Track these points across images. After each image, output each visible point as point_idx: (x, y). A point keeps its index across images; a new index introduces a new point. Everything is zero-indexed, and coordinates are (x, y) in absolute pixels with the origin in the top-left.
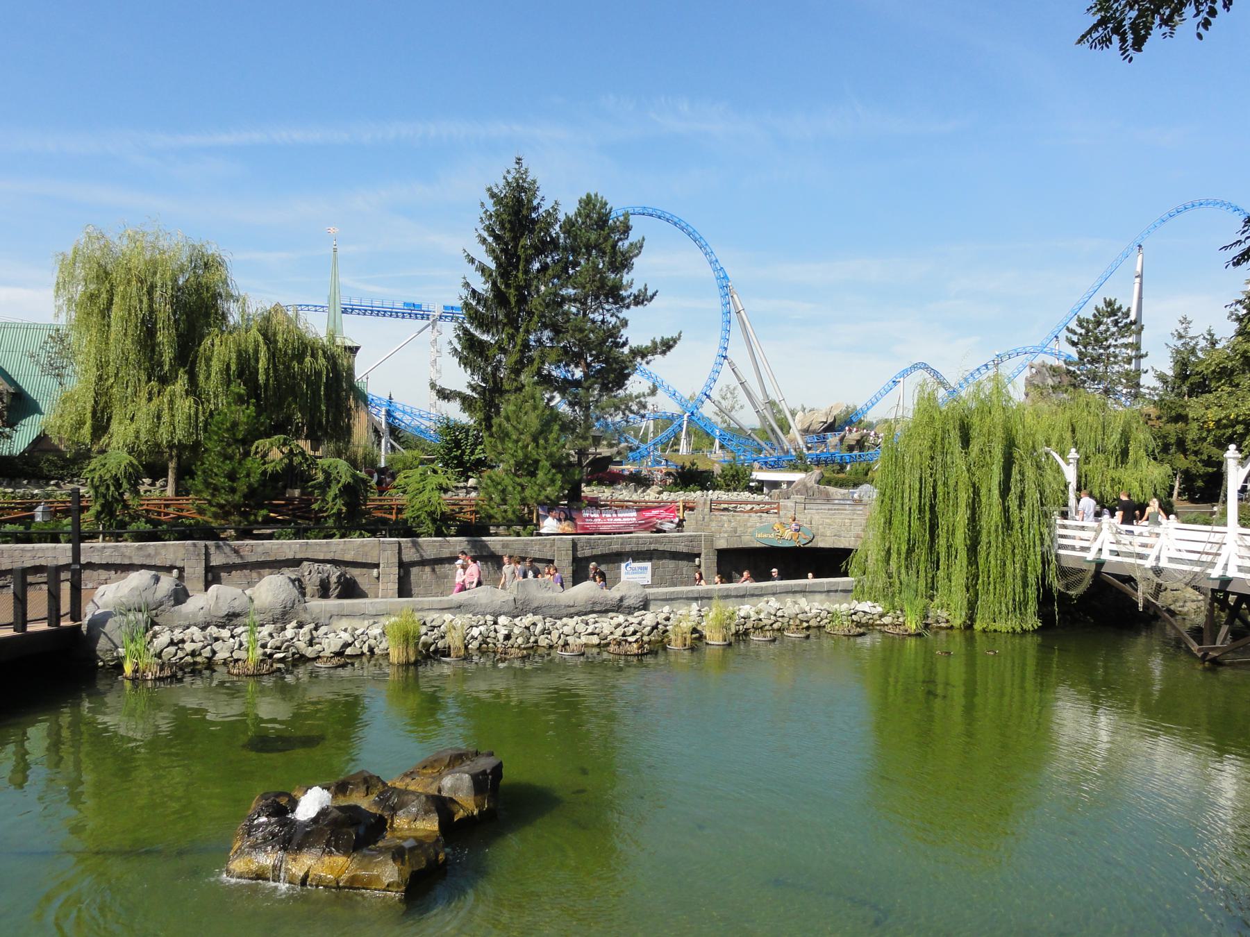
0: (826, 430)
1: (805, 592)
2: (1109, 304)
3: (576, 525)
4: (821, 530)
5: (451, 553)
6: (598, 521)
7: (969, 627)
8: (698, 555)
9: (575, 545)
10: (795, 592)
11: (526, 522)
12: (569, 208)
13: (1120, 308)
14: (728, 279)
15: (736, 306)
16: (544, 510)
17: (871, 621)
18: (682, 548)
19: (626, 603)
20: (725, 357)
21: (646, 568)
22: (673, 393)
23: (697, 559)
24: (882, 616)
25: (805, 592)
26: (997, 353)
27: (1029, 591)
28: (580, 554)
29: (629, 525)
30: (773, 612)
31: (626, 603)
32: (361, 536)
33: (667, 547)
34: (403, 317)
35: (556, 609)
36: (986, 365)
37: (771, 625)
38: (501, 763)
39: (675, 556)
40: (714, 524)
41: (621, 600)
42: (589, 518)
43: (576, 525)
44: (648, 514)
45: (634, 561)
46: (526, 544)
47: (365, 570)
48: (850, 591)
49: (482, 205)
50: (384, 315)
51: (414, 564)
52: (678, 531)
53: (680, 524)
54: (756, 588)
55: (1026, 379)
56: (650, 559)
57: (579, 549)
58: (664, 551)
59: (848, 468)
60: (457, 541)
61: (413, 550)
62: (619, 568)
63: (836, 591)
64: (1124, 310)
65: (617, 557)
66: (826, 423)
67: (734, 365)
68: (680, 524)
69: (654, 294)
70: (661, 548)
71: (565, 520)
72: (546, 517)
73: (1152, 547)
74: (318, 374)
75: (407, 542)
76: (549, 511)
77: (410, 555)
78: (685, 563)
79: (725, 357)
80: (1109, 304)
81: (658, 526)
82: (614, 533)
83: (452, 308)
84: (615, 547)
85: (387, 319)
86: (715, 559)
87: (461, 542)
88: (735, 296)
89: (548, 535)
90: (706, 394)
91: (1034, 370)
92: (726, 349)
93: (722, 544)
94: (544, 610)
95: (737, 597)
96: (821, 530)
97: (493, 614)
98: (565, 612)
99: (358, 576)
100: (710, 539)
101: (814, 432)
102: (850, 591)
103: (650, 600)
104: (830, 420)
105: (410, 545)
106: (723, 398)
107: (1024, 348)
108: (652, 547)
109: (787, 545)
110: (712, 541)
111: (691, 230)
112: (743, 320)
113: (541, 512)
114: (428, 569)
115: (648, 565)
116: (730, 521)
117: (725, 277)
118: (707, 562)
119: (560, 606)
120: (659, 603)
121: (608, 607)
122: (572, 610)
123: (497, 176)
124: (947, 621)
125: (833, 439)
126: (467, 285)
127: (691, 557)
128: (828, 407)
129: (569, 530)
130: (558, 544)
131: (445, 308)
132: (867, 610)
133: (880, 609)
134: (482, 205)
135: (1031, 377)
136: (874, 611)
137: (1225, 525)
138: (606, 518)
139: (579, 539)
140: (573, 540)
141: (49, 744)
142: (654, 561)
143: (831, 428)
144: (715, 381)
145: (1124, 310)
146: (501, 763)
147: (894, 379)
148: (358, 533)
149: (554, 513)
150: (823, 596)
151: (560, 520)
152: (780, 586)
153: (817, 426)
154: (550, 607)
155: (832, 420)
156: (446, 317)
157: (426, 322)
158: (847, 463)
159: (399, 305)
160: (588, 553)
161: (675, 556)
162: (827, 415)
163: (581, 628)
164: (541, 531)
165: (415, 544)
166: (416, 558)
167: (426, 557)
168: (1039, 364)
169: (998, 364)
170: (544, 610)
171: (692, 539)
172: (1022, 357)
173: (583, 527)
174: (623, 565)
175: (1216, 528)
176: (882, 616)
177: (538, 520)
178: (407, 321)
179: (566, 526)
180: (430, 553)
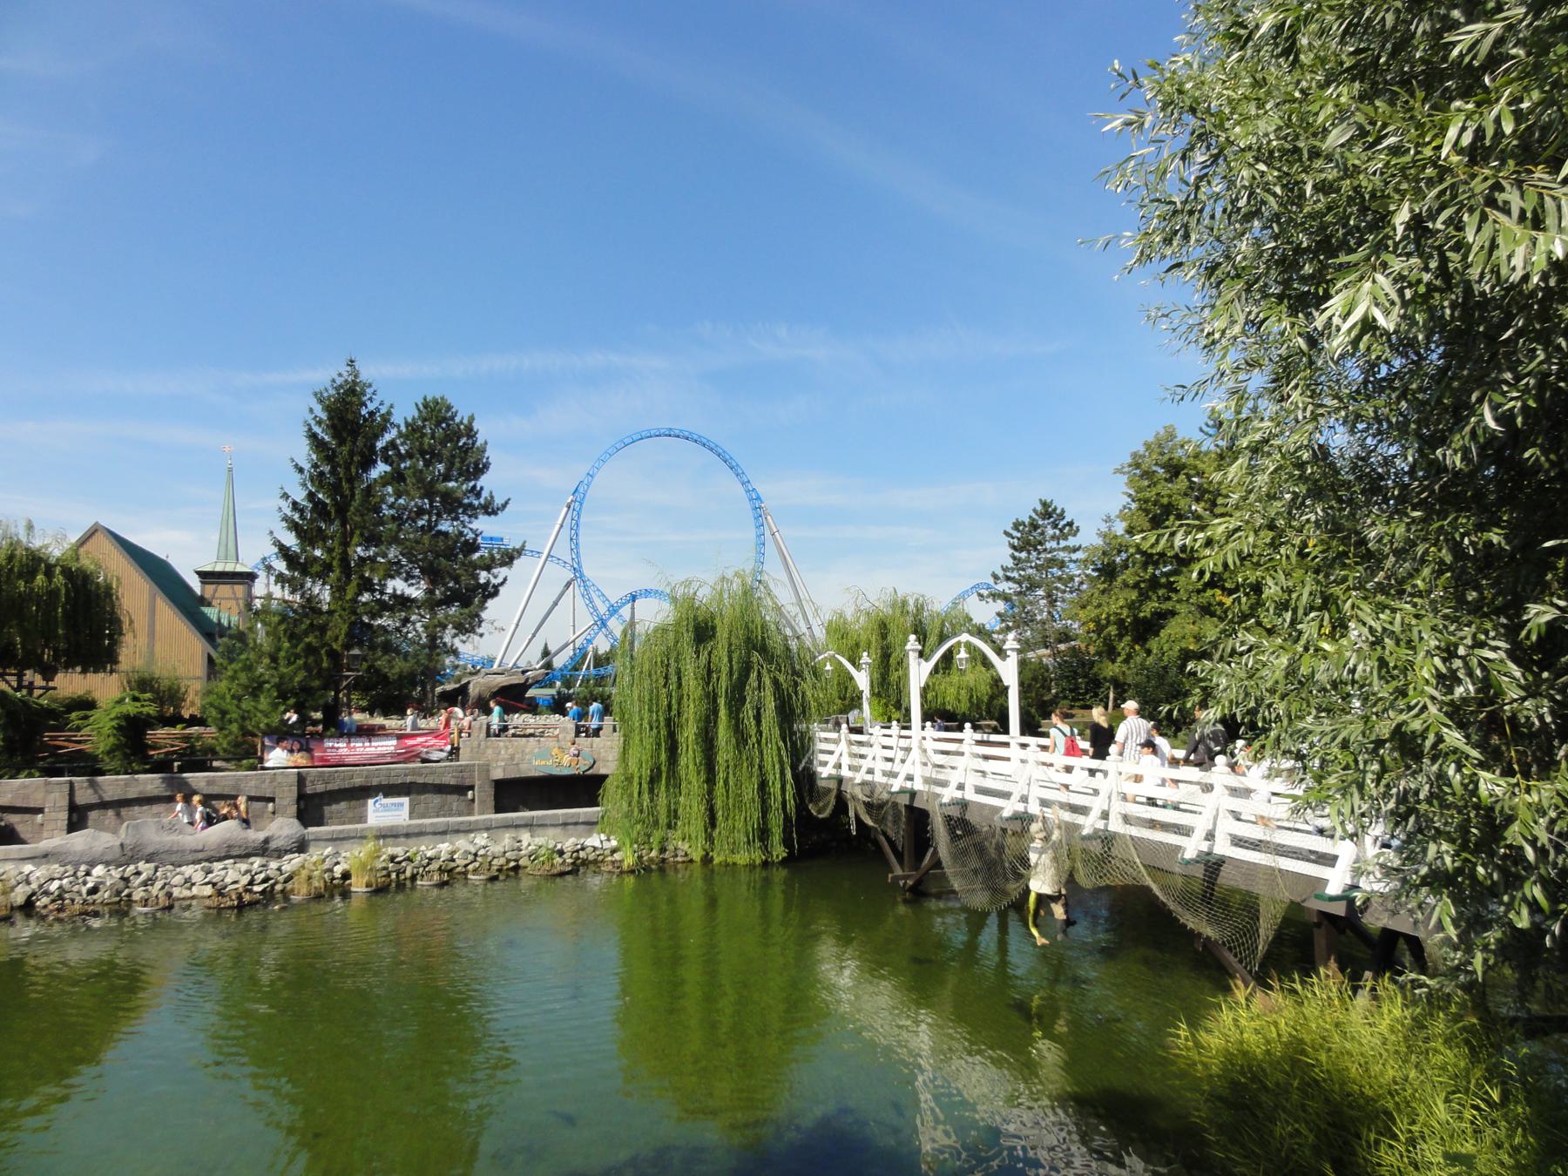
1: (531, 825)
2: (1045, 504)
3: (312, 758)
4: (603, 754)
5: (140, 793)
6: (344, 751)
7: (707, 860)
8: (472, 788)
9: (301, 780)
10: (517, 826)
11: (246, 753)
12: (404, 412)
13: (1055, 509)
15: (770, 529)
16: (271, 741)
17: (600, 858)
18: (449, 779)
19: (273, 845)
21: (402, 805)
23: (470, 793)
24: (614, 851)
25: (531, 825)
27: (771, 816)
28: (309, 790)
29: (383, 755)
30: (473, 851)
31: (273, 845)
32: (30, 775)
33: (429, 780)
35: (180, 854)
37: (466, 866)
39: (441, 789)
40: (489, 751)
41: (267, 841)
42: (333, 748)
43: (312, 758)
44: (410, 742)
45: (386, 796)
46: (239, 779)
47: (27, 817)
48: (595, 823)
49: (311, 410)
51: (91, 807)
52: (451, 760)
53: (455, 752)
54: (462, 823)
56: (407, 794)
57: (308, 783)
58: (425, 785)
60: (148, 779)
61: (90, 791)
62: (365, 805)
63: (576, 824)
64: (1058, 511)
65: (363, 792)
68: (455, 752)
69: (507, 503)
70: (420, 780)
71: (299, 751)
72: (274, 748)
73: (831, 753)
74: (53, 594)
75: (82, 782)
76: (278, 742)
77: (84, 796)
78: (455, 797)
80: (1045, 504)
81: (424, 756)
82: (364, 765)
84: (358, 781)
86: (492, 792)
87: (153, 779)
89: (273, 768)
93: (498, 774)
94: (163, 856)
95: (435, 833)
96: (603, 754)
97: (87, 863)
98: (190, 858)
99: (19, 823)
100: (486, 769)
102: (595, 823)
103: (309, 841)
105: (86, 785)
108: (408, 779)
109: (566, 772)
110: (488, 771)
113: (267, 742)
114: (110, 813)
115: (405, 800)
116: (507, 748)
117: (758, 498)
118: (482, 794)
119: (183, 851)
120: (322, 843)
121: (250, 850)
122: (201, 855)
123: (326, 375)
124: (686, 855)
126: (286, 496)
127: (461, 790)
129: (303, 762)
130: (279, 779)
132: (598, 844)
133: (614, 843)
134: (311, 410)
136: (607, 845)
137: (1006, 732)
138: (354, 747)
139: (308, 773)
140: (299, 773)
141: (845, 940)
142: (413, 796)
145: (1058, 511)
148: (26, 772)
149: (284, 744)
150: (558, 830)
151: (291, 751)
152: (496, 819)
154: (169, 852)
160: (320, 788)
161: (441, 789)
163: (198, 877)
164: (267, 765)
165: (93, 785)
166: (94, 800)
167: (107, 798)
170: (163, 856)
171: (462, 769)
173: (322, 759)
174: (371, 802)
175: (994, 738)
176: (614, 851)
177: (263, 753)
179: (300, 759)
180: (110, 794)
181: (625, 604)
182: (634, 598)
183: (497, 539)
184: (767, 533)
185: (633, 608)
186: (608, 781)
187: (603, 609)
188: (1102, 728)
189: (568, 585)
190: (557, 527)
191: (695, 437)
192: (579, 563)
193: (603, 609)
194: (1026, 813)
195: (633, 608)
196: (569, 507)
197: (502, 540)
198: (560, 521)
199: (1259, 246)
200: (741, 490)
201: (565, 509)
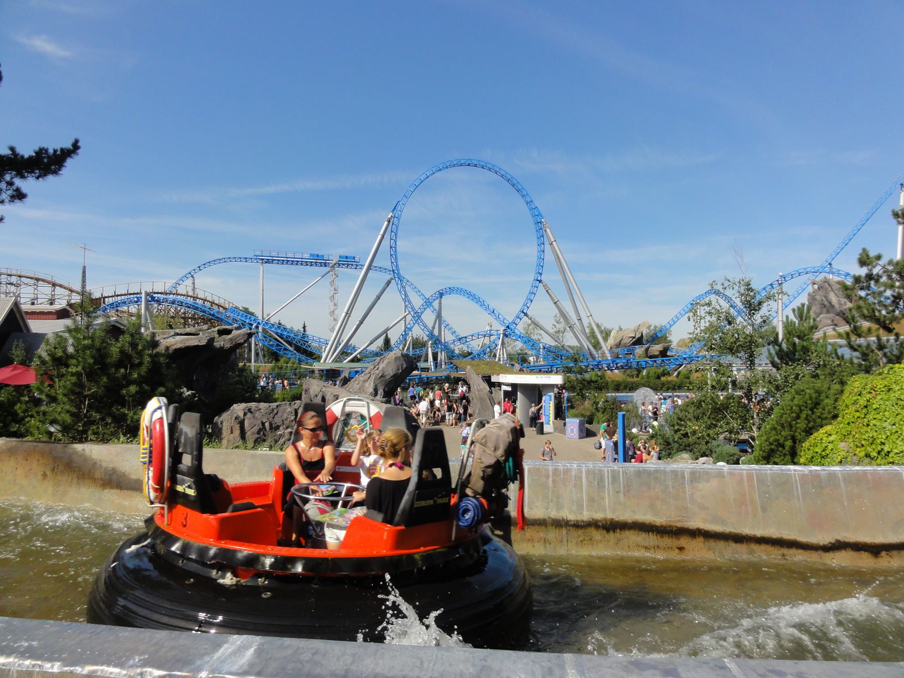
0: (635, 344)
14: (542, 216)
15: (549, 239)
20: (540, 281)
22: (492, 310)
26: (781, 274)
34: (311, 265)
36: (771, 285)
38: (864, 250)
50: (292, 264)
55: (809, 294)
59: (644, 372)
66: (634, 338)
67: (548, 287)
79: (540, 281)
83: (347, 257)
85: (285, 266)
88: (548, 230)
90: (523, 312)
91: (816, 287)
92: (541, 274)
101: (625, 346)
104: (638, 336)
106: (558, 322)
107: (806, 269)
111: (504, 173)
112: (557, 255)
117: (539, 215)
125: (639, 350)
128: (636, 325)
131: (340, 257)
135: (814, 292)
143: (639, 341)
144: (532, 301)
146: (864, 250)
147: (692, 302)
153: (627, 341)
155: (640, 335)
156: (343, 264)
157: (327, 269)
158: (643, 368)
159: (306, 256)
162: (635, 331)
168: (821, 281)
169: (782, 283)
172: (804, 278)
178: (314, 268)
181: (434, 300)
182: (441, 295)
183: (350, 258)
184: (546, 243)
185: (440, 303)
186: (155, 517)
187: (417, 302)
188: (274, 562)
189: (389, 283)
190: (380, 237)
191: (489, 166)
192: (397, 266)
193: (417, 302)
194: (824, 603)
195: (440, 303)
196: (389, 222)
197: (354, 258)
198: (382, 233)
199: (724, 409)
200: (524, 208)
201: (386, 223)
